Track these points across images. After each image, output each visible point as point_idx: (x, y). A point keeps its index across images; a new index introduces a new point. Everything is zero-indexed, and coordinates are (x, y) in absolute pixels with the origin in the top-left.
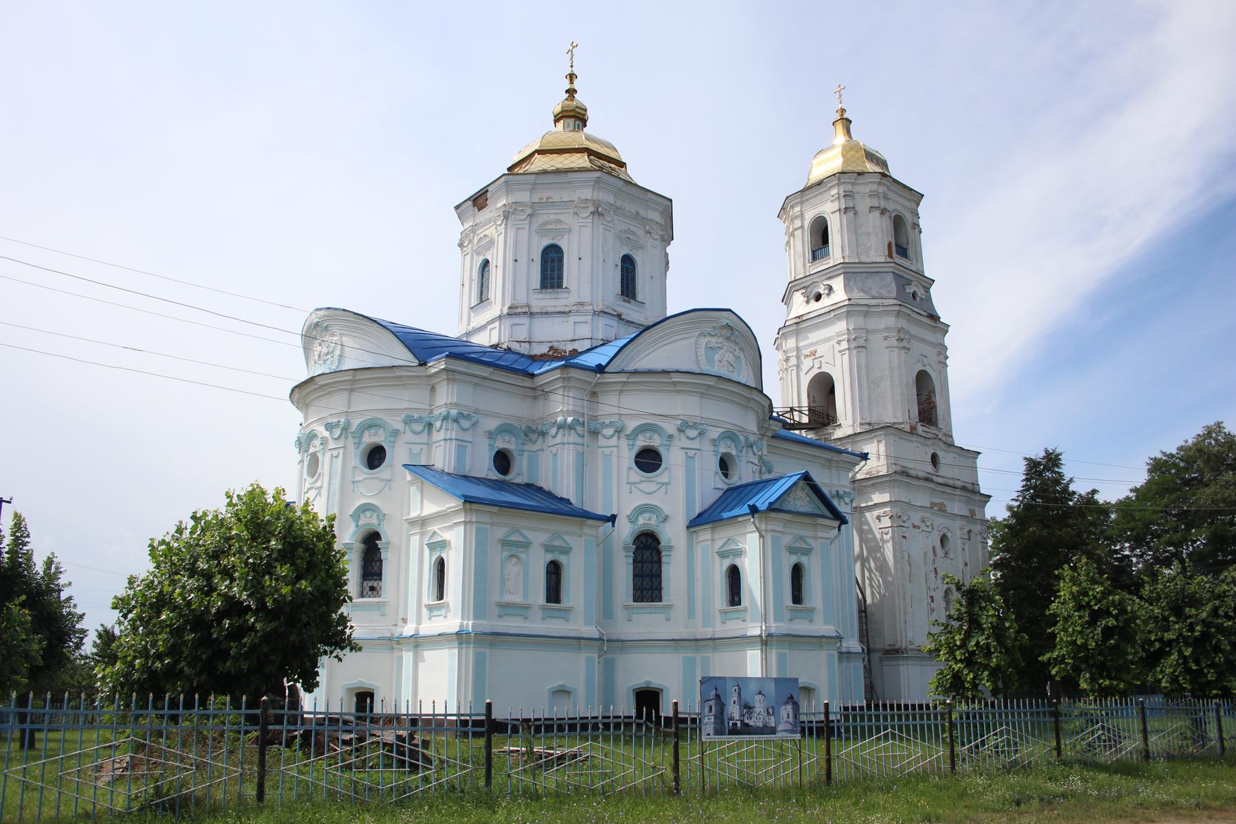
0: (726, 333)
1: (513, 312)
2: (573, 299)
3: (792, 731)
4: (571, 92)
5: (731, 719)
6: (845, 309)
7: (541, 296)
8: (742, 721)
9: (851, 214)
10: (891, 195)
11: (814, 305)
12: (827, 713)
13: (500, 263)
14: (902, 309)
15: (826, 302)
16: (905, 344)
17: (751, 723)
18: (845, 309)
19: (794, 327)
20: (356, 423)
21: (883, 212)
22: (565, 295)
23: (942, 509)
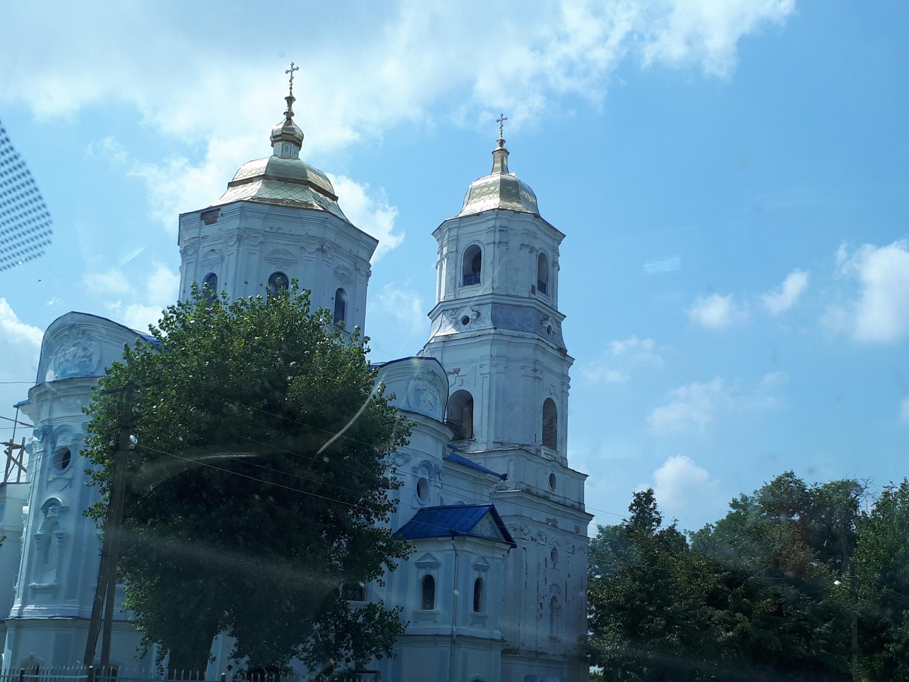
0: (430, 377)
4: (289, 114)
9: (503, 248)
10: (540, 235)
14: (540, 343)
16: (538, 374)
21: (532, 250)
23: (555, 526)
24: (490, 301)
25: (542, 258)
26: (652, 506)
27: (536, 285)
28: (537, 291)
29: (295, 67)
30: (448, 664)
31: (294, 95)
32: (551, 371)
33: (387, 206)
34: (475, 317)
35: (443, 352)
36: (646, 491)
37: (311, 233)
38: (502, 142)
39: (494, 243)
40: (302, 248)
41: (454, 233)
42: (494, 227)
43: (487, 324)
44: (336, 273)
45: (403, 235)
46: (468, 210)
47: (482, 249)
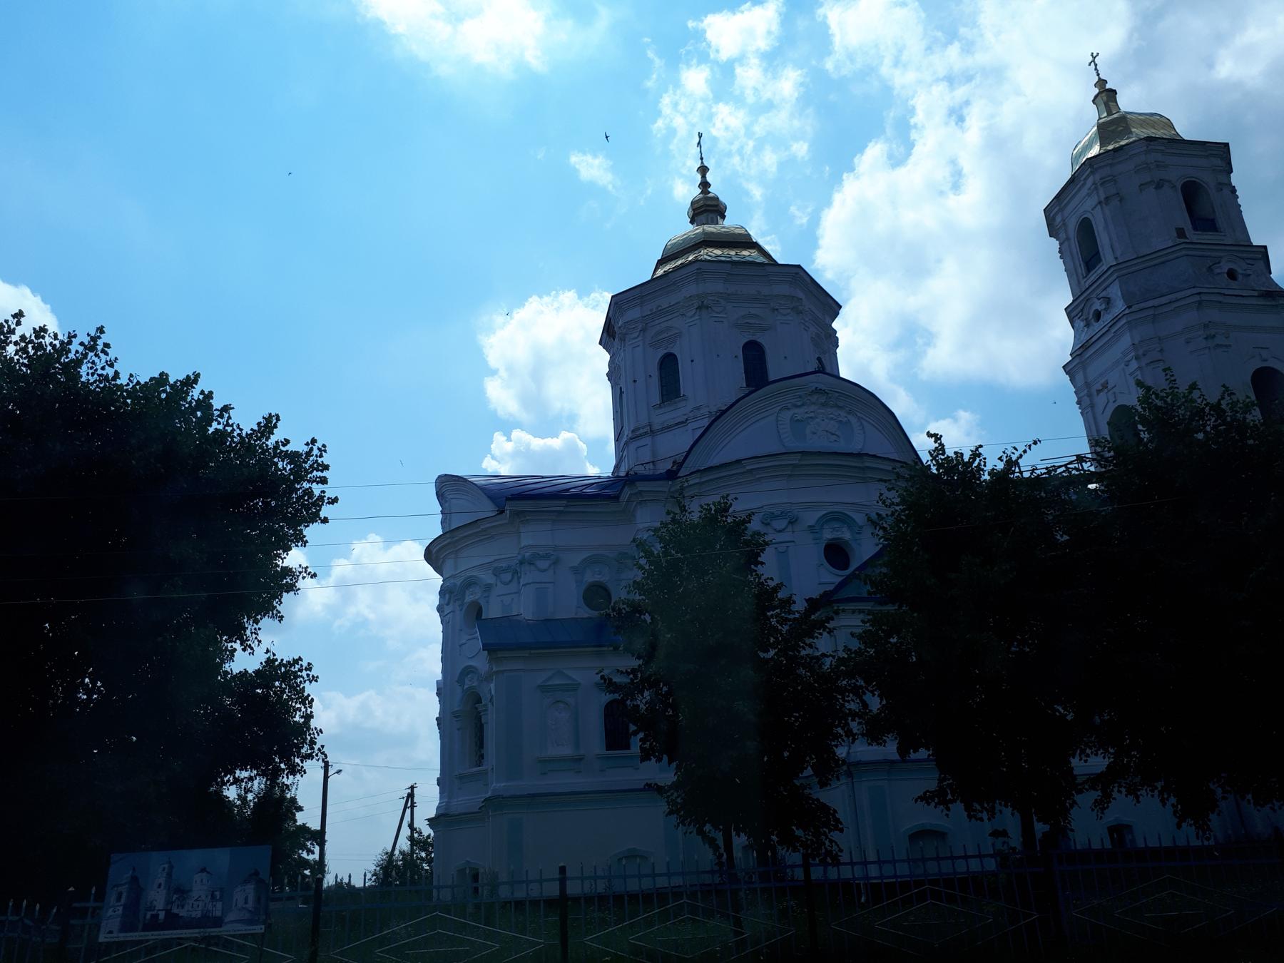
3: (250, 922)
4: (705, 185)
5: (151, 908)
7: (663, 410)
8: (168, 912)
11: (1097, 326)
12: (563, 881)
14: (1204, 297)
15: (1107, 318)
17: (183, 913)
31: (706, 164)
36: (157, 375)
40: (774, 310)
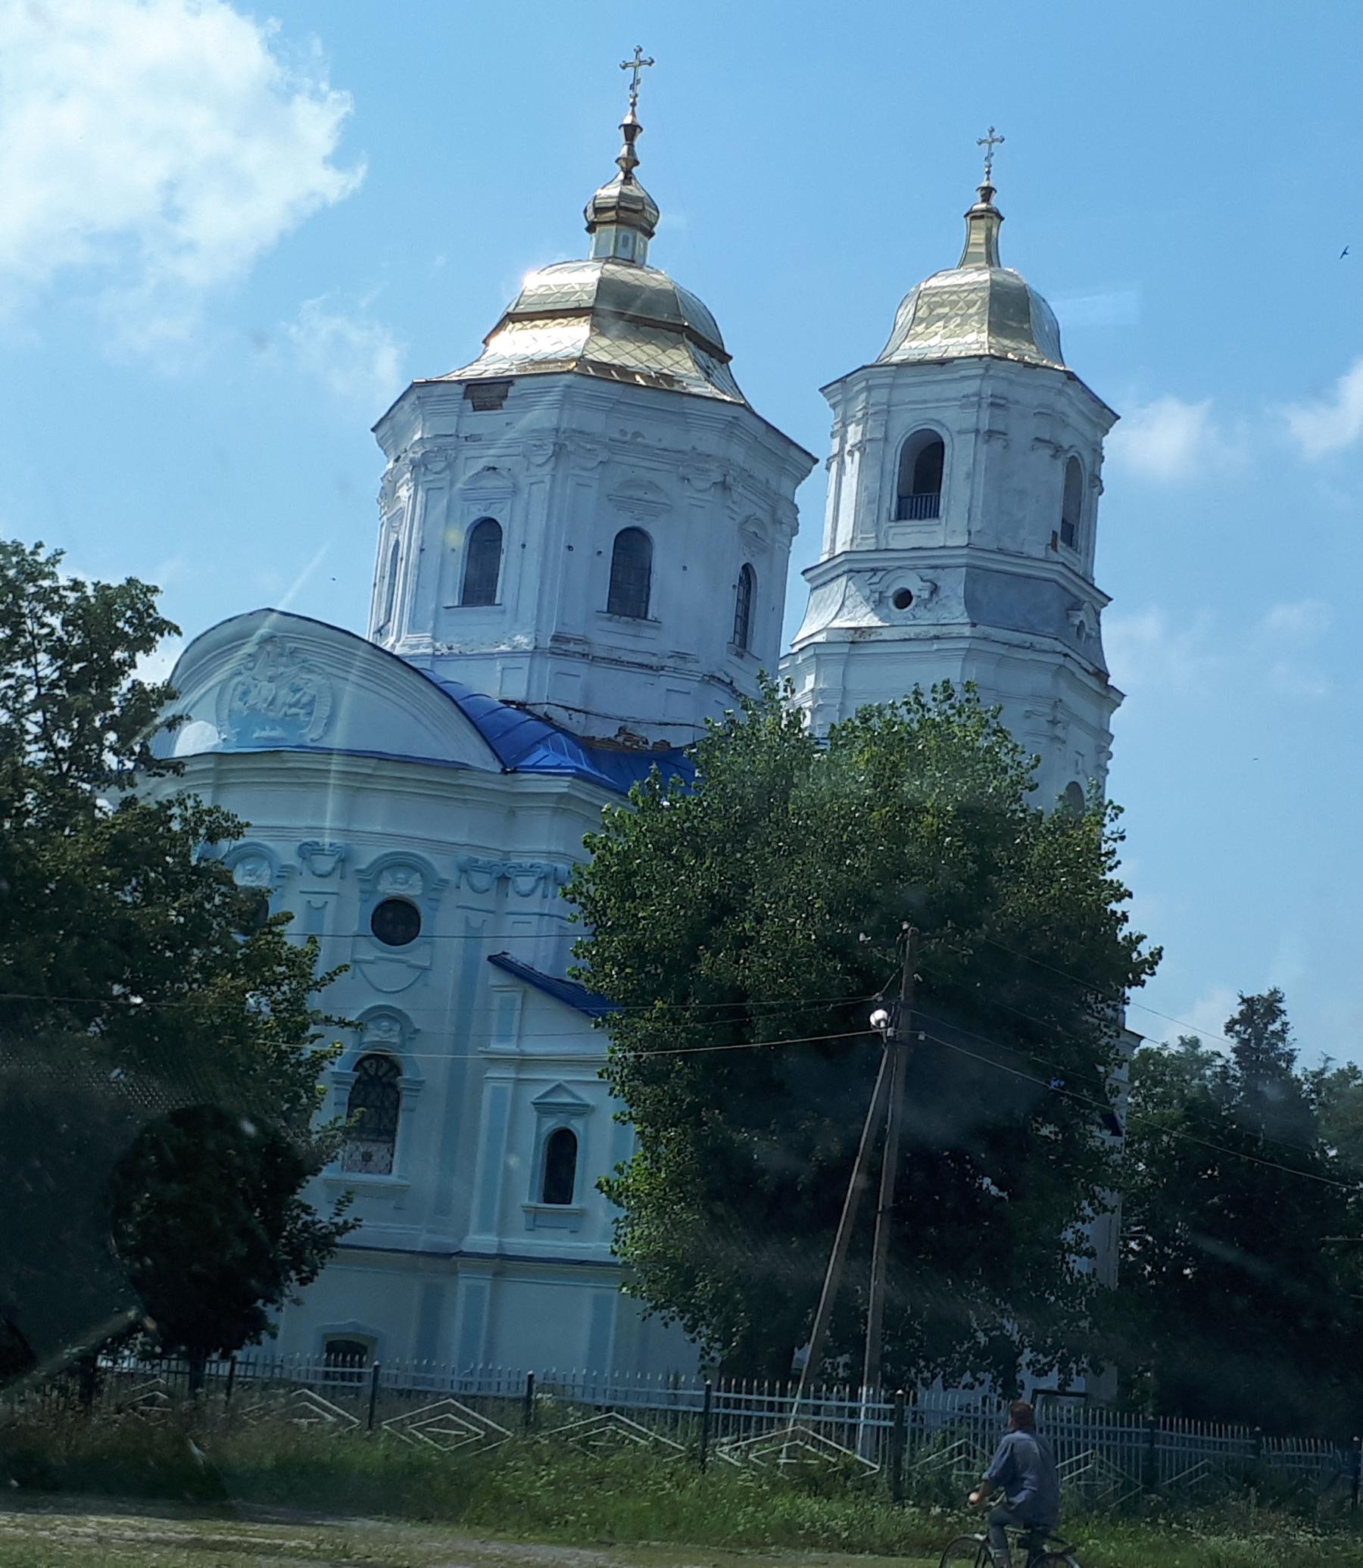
1: (560, 646)
2: (669, 645)
6: (964, 644)
9: (997, 444)
13: (534, 541)
16: (1059, 731)
18: (964, 644)
19: (845, 649)
20: (368, 855)
21: (1058, 450)
22: (649, 633)
24: (963, 561)
25: (1073, 467)
26: (1276, 1026)
27: (1059, 531)
28: (1060, 543)
29: (643, 56)
30: (485, 1319)
32: (1080, 721)
33: (324, 86)
34: (926, 595)
35: (846, 665)
37: (702, 447)
38: (987, 193)
39: (977, 432)
41: (880, 395)
42: (978, 394)
43: (955, 613)
44: (741, 528)
45: (362, 171)
46: (910, 349)
47: (946, 441)
